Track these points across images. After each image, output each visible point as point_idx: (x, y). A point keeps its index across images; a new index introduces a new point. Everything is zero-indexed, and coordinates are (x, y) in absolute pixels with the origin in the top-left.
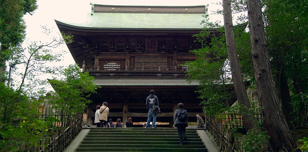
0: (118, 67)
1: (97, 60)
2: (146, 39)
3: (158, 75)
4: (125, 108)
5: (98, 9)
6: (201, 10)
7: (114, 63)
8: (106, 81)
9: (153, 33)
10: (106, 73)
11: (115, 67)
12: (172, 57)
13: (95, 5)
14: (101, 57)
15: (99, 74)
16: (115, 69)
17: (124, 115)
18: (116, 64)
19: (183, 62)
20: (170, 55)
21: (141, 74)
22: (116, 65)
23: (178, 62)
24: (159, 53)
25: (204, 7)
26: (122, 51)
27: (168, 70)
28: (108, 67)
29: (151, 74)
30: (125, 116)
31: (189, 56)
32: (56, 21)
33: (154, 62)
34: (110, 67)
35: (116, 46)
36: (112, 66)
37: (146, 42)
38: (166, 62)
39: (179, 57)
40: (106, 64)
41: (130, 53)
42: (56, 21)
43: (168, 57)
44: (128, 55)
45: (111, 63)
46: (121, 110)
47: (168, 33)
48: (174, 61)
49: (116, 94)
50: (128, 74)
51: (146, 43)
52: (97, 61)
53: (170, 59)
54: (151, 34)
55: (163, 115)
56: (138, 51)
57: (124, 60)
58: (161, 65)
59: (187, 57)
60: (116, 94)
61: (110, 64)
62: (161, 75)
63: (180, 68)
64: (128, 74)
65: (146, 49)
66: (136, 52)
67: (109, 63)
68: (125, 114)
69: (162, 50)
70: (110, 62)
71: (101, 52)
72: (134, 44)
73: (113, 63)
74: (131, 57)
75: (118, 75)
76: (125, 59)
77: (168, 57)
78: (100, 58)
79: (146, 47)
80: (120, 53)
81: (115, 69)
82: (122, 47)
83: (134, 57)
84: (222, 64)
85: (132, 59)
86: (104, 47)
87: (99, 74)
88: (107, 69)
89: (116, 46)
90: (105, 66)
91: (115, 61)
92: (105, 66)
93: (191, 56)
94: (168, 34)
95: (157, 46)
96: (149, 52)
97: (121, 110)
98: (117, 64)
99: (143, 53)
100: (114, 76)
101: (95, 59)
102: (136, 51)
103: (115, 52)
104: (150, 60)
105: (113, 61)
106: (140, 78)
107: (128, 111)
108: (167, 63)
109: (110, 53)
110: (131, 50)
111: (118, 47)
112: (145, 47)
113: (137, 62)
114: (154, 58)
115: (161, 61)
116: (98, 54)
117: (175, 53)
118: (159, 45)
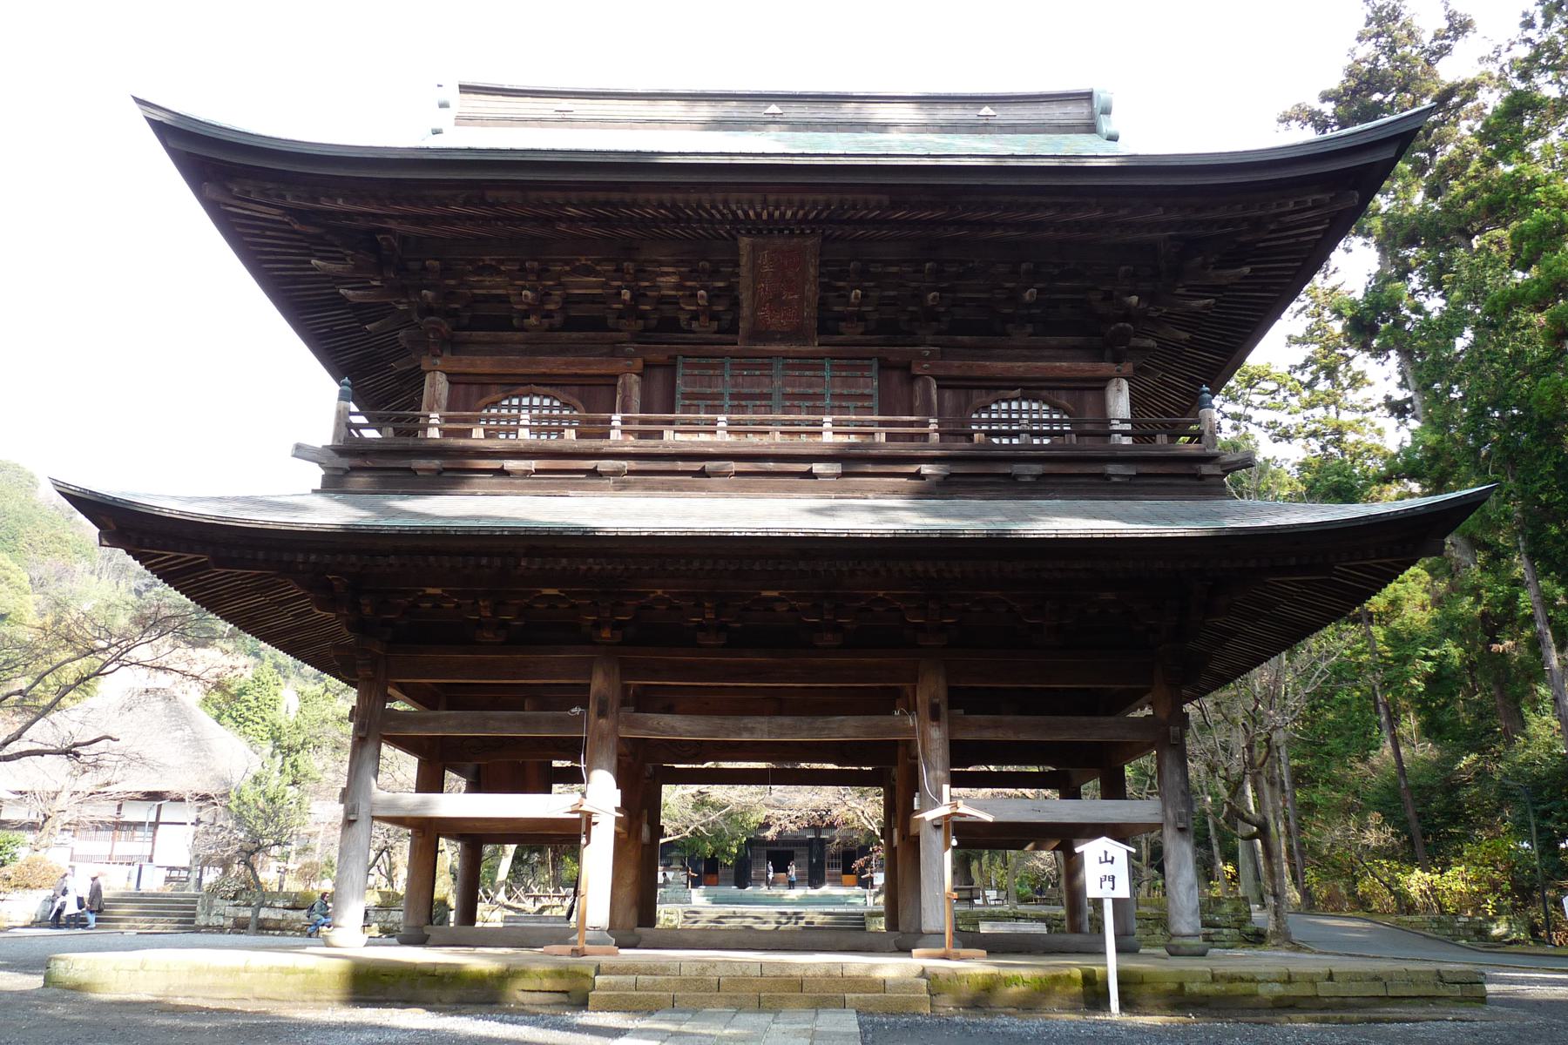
3: (1111, 469)
6: (1084, 108)
7: (547, 402)
12: (908, 368)
18: (556, 403)
19: (975, 392)
20: (895, 354)
22: (1045, 416)
23: (948, 394)
24: (824, 338)
25: (1088, 97)
26: (598, 324)
28: (1000, 421)
29: (771, 466)
30: (602, 738)
31: (1017, 359)
32: (230, 173)
33: (796, 390)
34: (1010, 421)
36: (1021, 419)
37: (744, 260)
38: (869, 397)
39: (956, 367)
40: (495, 404)
41: (640, 338)
42: (230, 173)
43: (885, 366)
44: (630, 348)
45: (526, 401)
46: (579, 695)
48: (918, 387)
49: (430, 591)
51: (744, 270)
52: (438, 385)
53: (895, 377)
55: (850, 732)
56: (695, 325)
59: (1000, 365)
61: (510, 407)
63: (1101, 429)
65: (745, 311)
67: (515, 402)
68: (602, 721)
69: (843, 320)
73: (536, 401)
74: (647, 365)
76: (616, 377)
77: (881, 367)
78: (456, 369)
79: (745, 296)
80: (582, 335)
82: (592, 299)
83: (670, 367)
85: (659, 376)
86: (487, 299)
87: (436, 463)
88: (990, 434)
90: (980, 422)
91: (547, 390)
92: (980, 422)
93: (1027, 359)
95: (811, 290)
96: (760, 334)
98: (565, 405)
99: (729, 337)
101: (423, 374)
102: (683, 324)
103: (551, 329)
104: (767, 380)
105: (535, 388)
106: (701, 489)
107: (624, 703)
109: (519, 335)
111: (568, 300)
112: (735, 304)
113: (686, 396)
115: (837, 391)
116: (455, 346)
117: (929, 338)
118: (824, 287)
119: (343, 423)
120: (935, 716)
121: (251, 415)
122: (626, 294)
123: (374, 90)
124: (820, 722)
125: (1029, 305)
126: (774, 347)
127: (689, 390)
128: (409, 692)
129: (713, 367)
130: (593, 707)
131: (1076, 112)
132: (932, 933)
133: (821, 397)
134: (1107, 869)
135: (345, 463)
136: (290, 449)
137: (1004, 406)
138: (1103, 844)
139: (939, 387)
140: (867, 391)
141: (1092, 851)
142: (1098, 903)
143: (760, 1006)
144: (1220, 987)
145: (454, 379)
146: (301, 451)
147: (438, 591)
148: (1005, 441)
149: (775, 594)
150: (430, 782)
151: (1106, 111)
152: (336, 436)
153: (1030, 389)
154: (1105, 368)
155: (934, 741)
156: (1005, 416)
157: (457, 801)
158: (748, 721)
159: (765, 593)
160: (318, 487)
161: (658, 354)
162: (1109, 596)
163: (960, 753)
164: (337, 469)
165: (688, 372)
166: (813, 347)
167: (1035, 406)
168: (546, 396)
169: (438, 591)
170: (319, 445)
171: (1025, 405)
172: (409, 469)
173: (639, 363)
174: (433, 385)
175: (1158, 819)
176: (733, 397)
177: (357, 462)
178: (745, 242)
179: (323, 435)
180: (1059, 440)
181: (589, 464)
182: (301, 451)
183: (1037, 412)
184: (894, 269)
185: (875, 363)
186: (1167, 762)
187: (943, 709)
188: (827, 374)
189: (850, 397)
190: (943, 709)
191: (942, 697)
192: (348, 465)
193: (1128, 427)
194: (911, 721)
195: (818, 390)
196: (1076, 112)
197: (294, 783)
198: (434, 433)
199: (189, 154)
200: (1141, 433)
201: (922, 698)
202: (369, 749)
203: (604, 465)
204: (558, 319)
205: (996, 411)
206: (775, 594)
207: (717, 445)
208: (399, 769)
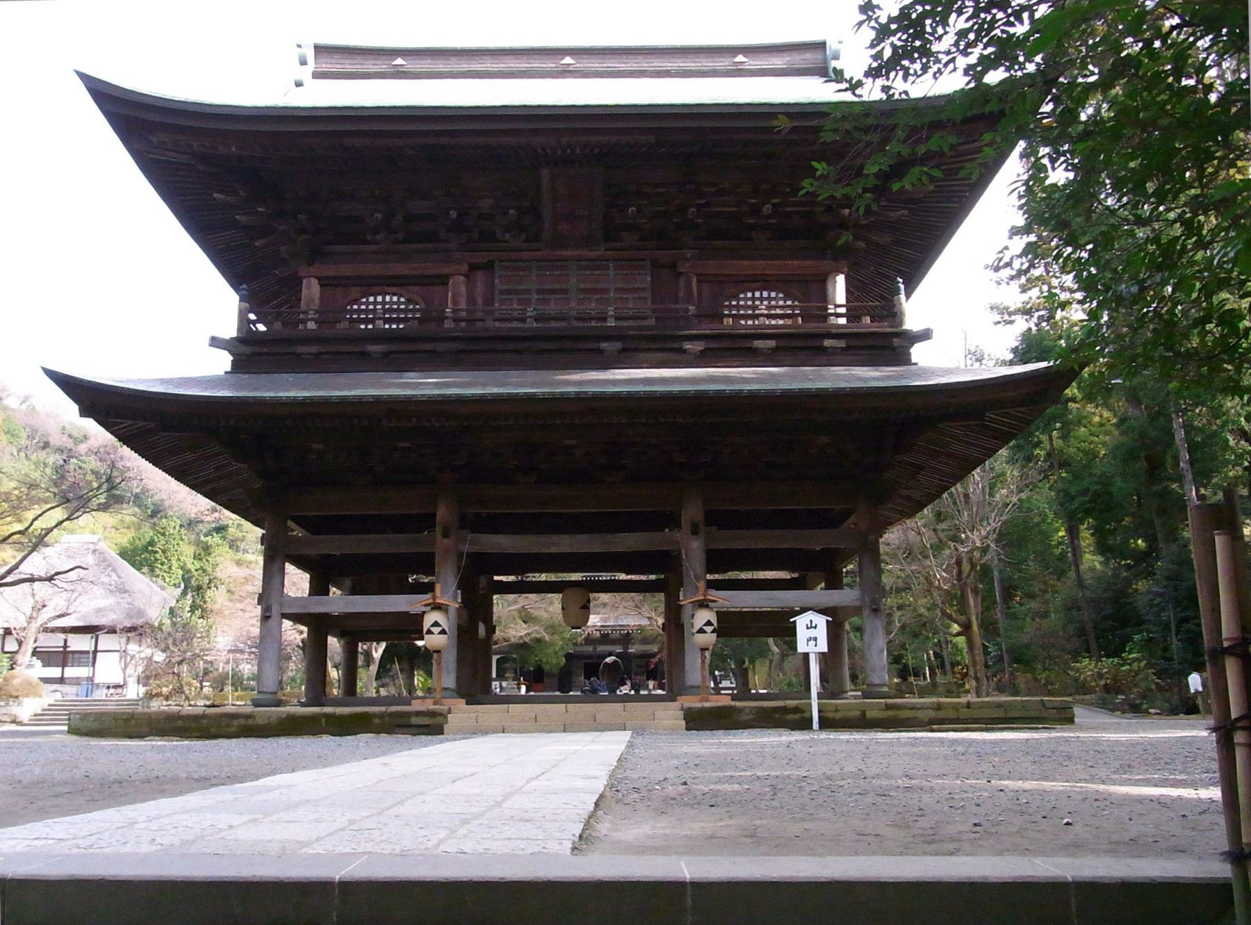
0: (414, 311)
1: (314, 282)
2: (545, 172)
3: (604, 345)
4: (443, 513)
5: (335, 58)
6: (813, 57)
8: (344, 378)
9: (576, 131)
10: (348, 340)
11: (398, 311)
12: (673, 266)
13: (320, 50)
14: (330, 270)
15: (314, 349)
16: (405, 320)
17: (441, 545)
18: (402, 300)
21: (520, 346)
22: (781, 303)
25: (822, 46)
26: (432, 237)
27: (652, 322)
28: (746, 307)
32: (84, 77)
35: (399, 217)
36: (383, 307)
40: (356, 301)
42: (84, 77)
43: (656, 265)
47: (650, 130)
48: (682, 282)
49: (402, 445)
50: (462, 346)
52: (311, 290)
54: (565, 140)
56: (507, 236)
57: (443, 280)
58: (620, 296)
60: (402, 445)
62: (619, 345)
64: (462, 346)
66: (499, 241)
68: (445, 540)
70: (375, 295)
71: (330, 244)
72: (485, 204)
74: (473, 268)
75: (404, 351)
76: (448, 276)
81: (398, 321)
84: (419, 648)
85: (480, 277)
87: (314, 349)
89: (399, 217)
90: (730, 307)
91: (395, 289)
92: (730, 307)
94: (651, 138)
97: (427, 521)
100: (387, 354)
107: (462, 527)
108: (648, 295)
109: (372, 248)
110: (476, 235)
113: (502, 292)
114: (586, 268)
115: (619, 286)
116: (316, 255)
119: (243, 321)
120: (695, 531)
121: (177, 317)
122: (453, 214)
123: (253, 69)
124: (610, 537)
125: (768, 217)
126: (569, 253)
127: (505, 287)
128: (300, 522)
129: (524, 269)
130: (438, 529)
131: (810, 58)
132: (693, 687)
133: (607, 291)
134: (812, 633)
135: (248, 350)
136: (207, 341)
137: (749, 295)
138: (809, 616)
139: (698, 281)
140: (643, 285)
141: (801, 621)
142: (806, 655)
143: (637, 853)
144: (891, 713)
145: (324, 283)
146: (215, 342)
147: (321, 446)
148: (750, 322)
149: (574, 442)
150: (319, 588)
151: (836, 57)
152: (239, 330)
153: (766, 283)
154: (827, 264)
155: (694, 551)
156: (750, 303)
157: (338, 601)
158: (555, 538)
159: (566, 442)
160: (229, 369)
161: (481, 258)
162: (824, 439)
163: (716, 560)
164: (241, 355)
165: (504, 273)
166: (600, 252)
167: (773, 294)
168: (394, 294)
169: (321, 446)
170: (228, 337)
171: (765, 294)
172: (294, 354)
173: (465, 268)
174: (308, 288)
175: (857, 603)
176: (539, 292)
177: (257, 349)
178: (545, 172)
179: (230, 330)
180: (789, 322)
181: (429, 346)
182: (215, 342)
183: (774, 299)
184: (661, 190)
185: (648, 263)
186: (865, 560)
187: (702, 527)
188: (611, 272)
189: (628, 290)
190: (702, 527)
191: (700, 517)
192: (249, 353)
193: (843, 310)
194: (678, 535)
195: (606, 286)
196: (810, 58)
197: (202, 617)
198: (311, 325)
199: (154, 160)
200: (852, 315)
201: (685, 519)
202: (275, 567)
203: (441, 347)
204: (400, 236)
205: (743, 299)
206: (574, 442)
207: (525, 330)
208: (297, 581)
